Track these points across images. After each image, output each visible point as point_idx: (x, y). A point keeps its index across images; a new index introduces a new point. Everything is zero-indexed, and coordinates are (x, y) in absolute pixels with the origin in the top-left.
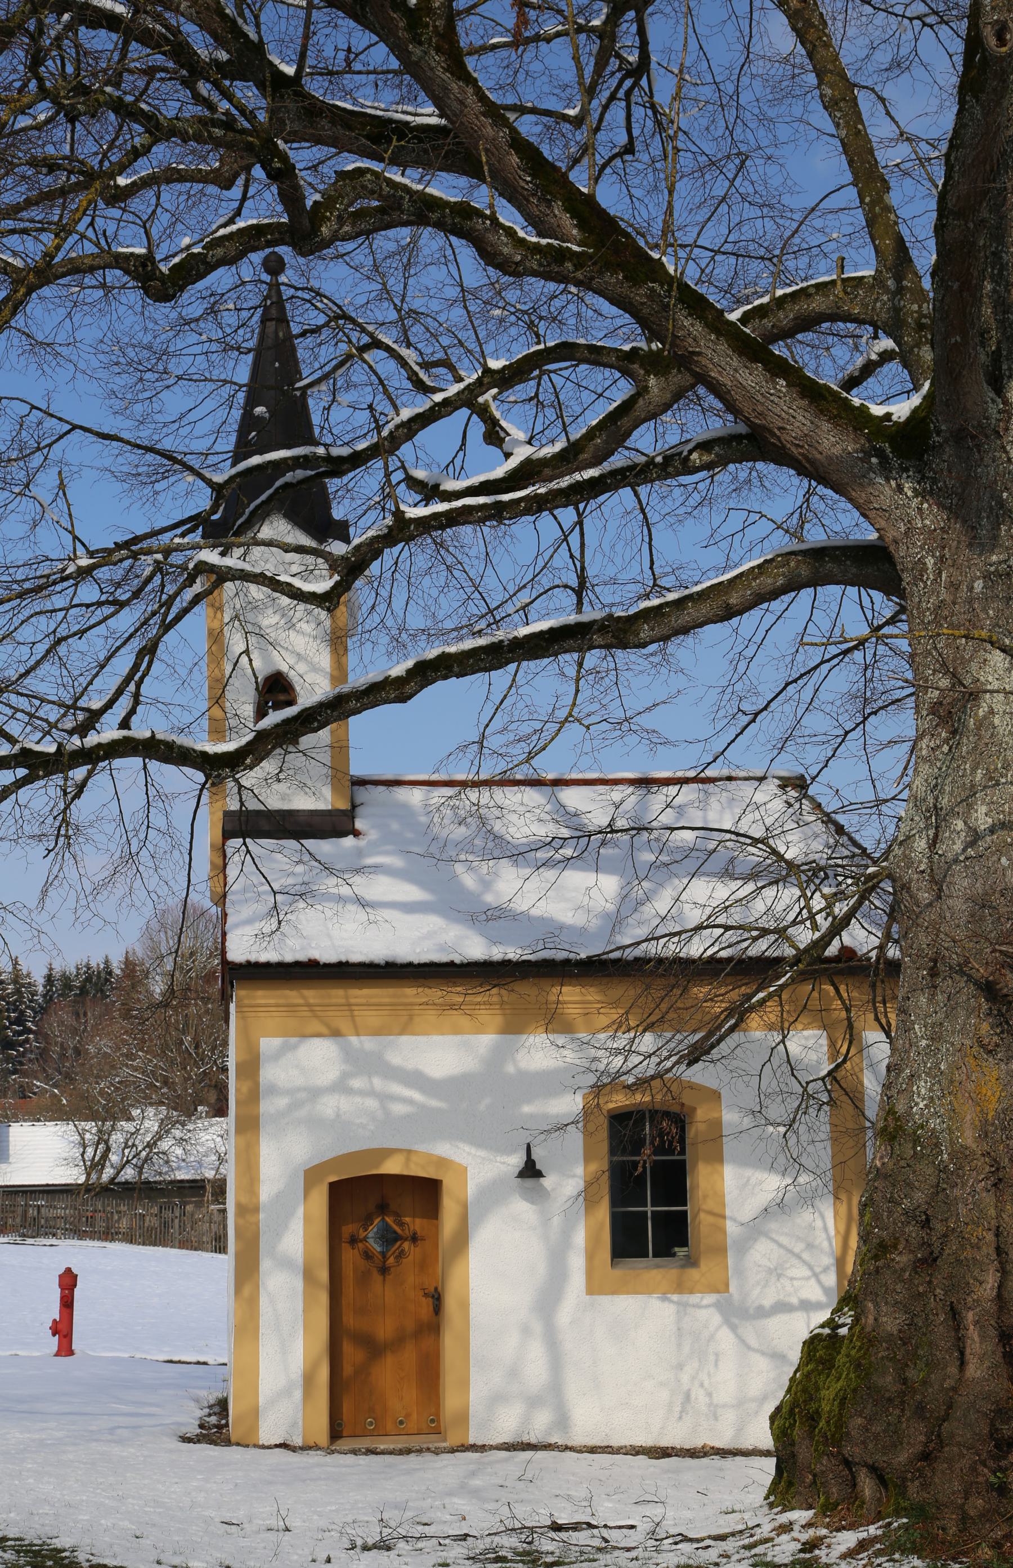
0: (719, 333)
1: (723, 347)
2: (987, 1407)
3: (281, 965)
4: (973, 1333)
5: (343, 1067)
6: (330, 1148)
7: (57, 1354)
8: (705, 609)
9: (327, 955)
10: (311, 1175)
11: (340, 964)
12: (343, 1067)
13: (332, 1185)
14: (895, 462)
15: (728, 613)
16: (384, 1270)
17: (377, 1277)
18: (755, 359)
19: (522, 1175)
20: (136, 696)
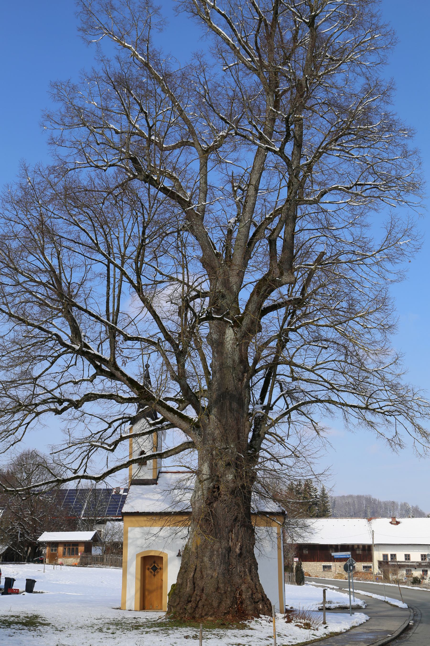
0: (164, 408)
1: (165, 410)
2: (188, 595)
3: (131, 513)
4: (188, 583)
5: (399, 504)
6: (139, 550)
7: (14, 580)
8: (173, 452)
9: (141, 511)
10: (137, 555)
11: (143, 513)
12: (399, 504)
13: (142, 557)
14: (196, 429)
15: (177, 453)
16: (154, 575)
17: (153, 577)
18: (171, 412)
19: (177, 556)
20: (86, 466)
